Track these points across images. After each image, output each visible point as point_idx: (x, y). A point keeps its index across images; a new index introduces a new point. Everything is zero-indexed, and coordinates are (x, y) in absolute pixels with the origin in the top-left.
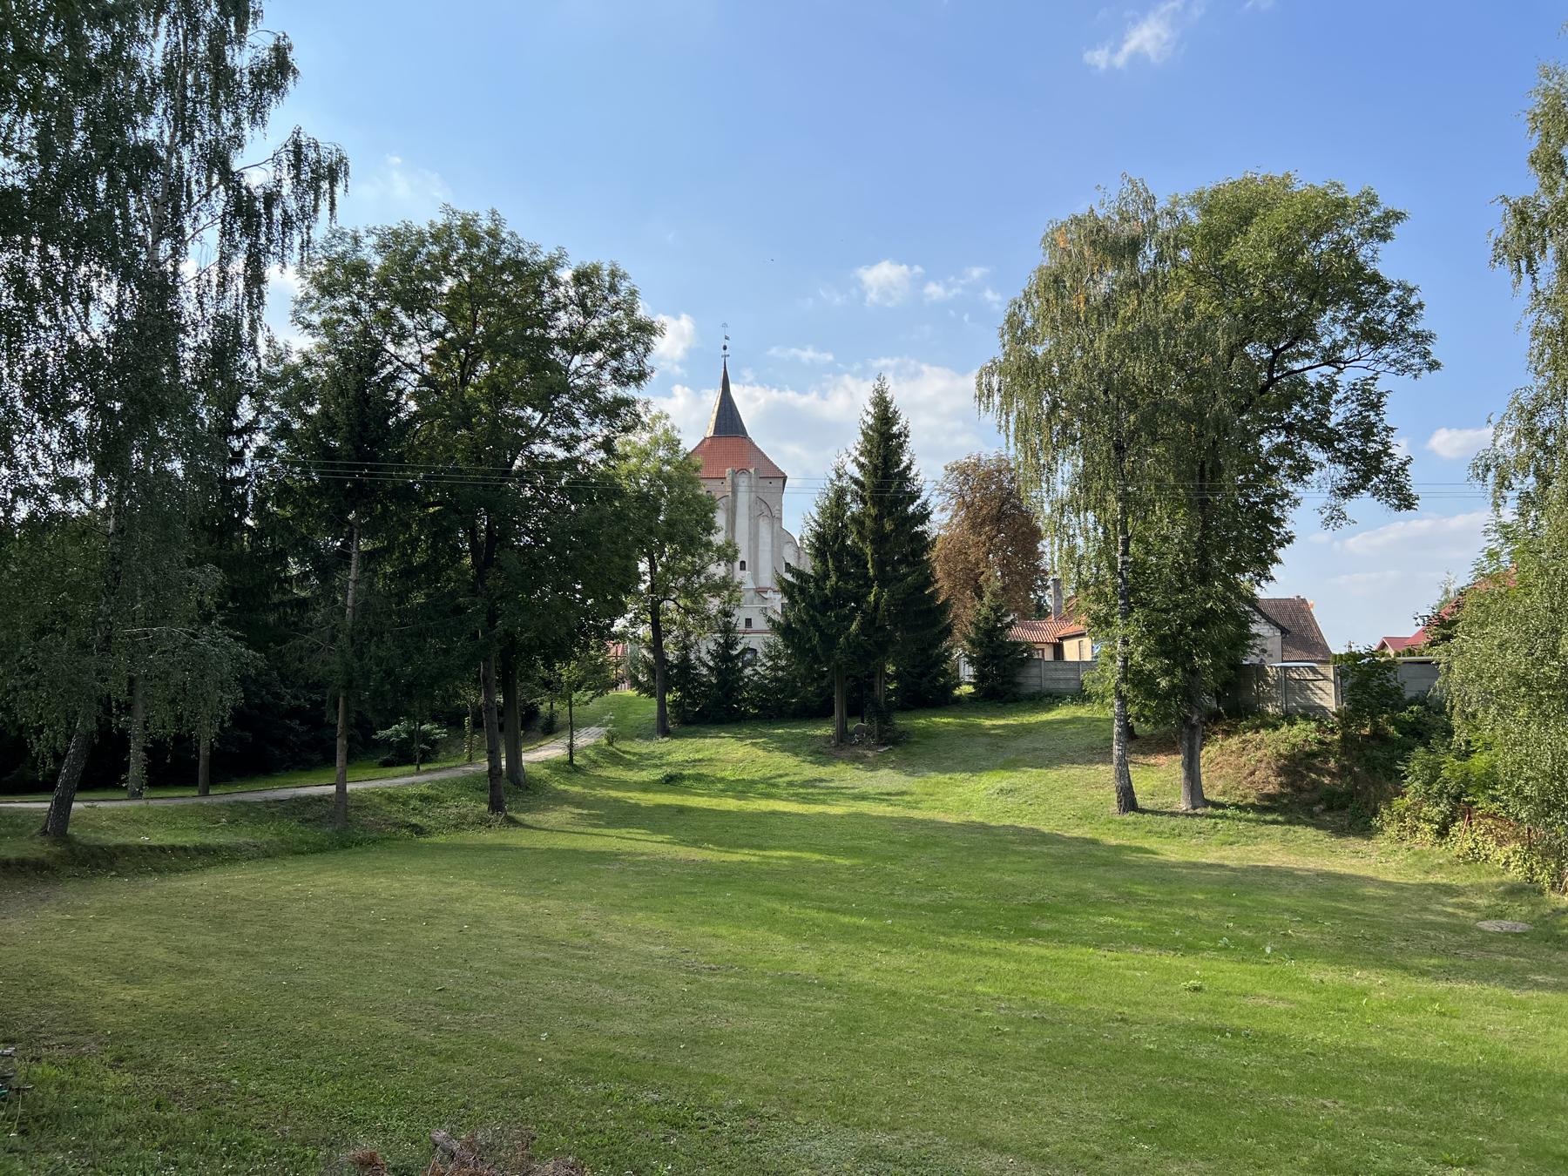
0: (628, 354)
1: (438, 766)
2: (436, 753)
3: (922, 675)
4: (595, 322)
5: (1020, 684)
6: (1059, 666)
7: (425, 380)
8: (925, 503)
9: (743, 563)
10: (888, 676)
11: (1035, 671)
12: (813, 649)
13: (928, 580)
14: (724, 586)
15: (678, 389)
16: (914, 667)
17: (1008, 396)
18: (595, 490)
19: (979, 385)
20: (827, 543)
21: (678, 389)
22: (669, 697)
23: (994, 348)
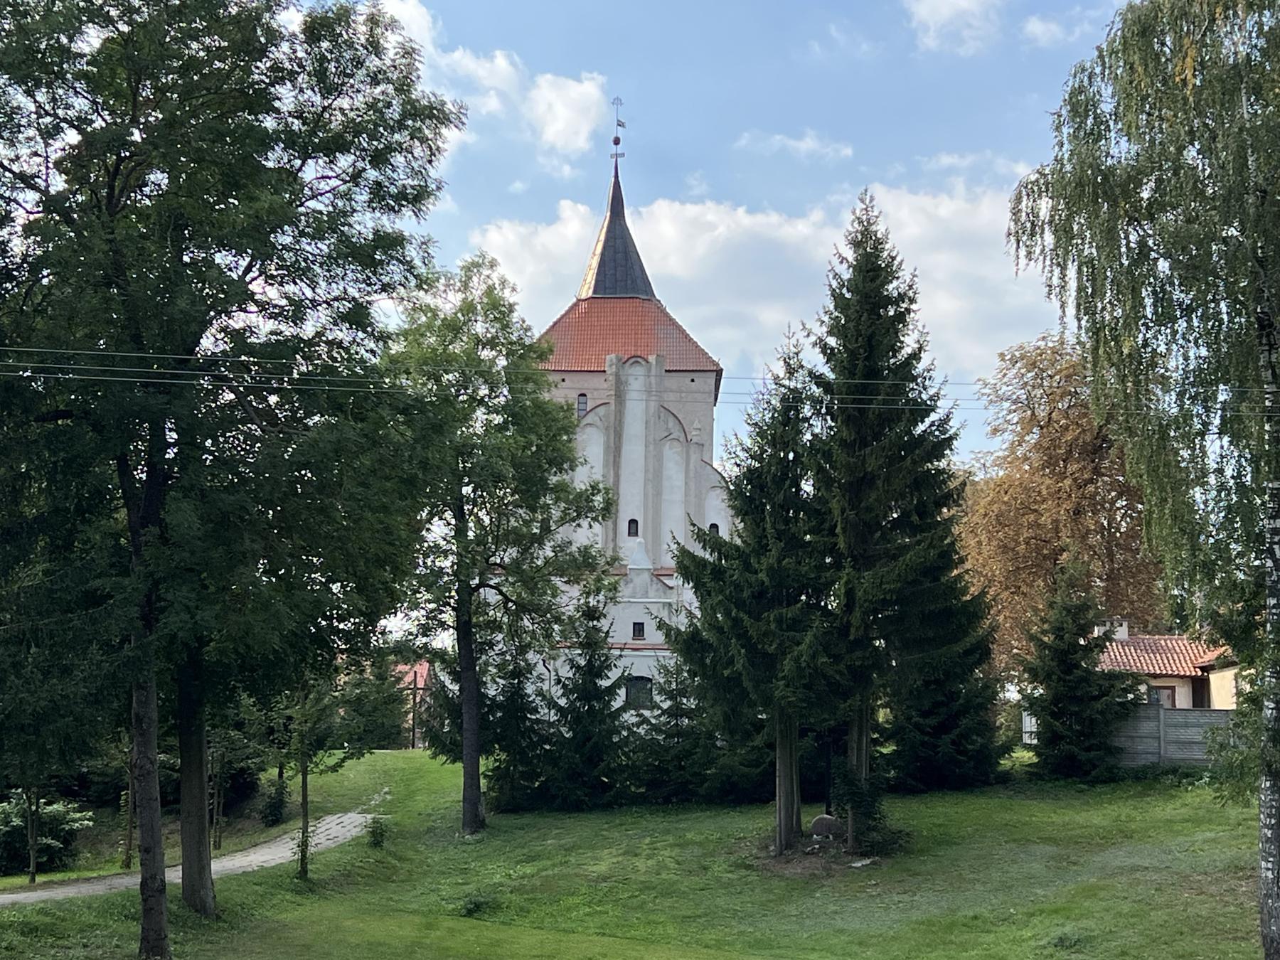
0: (399, 159)
1: (74, 876)
2: (74, 855)
3: (943, 728)
4: (344, 102)
5: (1120, 750)
6: (1196, 716)
7: (50, 203)
8: (946, 420)
9: (633, 523)
10: (877, 727)
11: (1146, 727)
12: (736, 680)
13: (947, 557)
14: (580, 565)
15: (566, 206)
16: (925, 714)
17: (1064, 233)
18: (351, 394)
19: (1016, 212)
20: (759, 491)
21: (566, 206)
22: (485, 764)
23: (1041, 148)
